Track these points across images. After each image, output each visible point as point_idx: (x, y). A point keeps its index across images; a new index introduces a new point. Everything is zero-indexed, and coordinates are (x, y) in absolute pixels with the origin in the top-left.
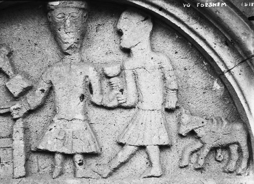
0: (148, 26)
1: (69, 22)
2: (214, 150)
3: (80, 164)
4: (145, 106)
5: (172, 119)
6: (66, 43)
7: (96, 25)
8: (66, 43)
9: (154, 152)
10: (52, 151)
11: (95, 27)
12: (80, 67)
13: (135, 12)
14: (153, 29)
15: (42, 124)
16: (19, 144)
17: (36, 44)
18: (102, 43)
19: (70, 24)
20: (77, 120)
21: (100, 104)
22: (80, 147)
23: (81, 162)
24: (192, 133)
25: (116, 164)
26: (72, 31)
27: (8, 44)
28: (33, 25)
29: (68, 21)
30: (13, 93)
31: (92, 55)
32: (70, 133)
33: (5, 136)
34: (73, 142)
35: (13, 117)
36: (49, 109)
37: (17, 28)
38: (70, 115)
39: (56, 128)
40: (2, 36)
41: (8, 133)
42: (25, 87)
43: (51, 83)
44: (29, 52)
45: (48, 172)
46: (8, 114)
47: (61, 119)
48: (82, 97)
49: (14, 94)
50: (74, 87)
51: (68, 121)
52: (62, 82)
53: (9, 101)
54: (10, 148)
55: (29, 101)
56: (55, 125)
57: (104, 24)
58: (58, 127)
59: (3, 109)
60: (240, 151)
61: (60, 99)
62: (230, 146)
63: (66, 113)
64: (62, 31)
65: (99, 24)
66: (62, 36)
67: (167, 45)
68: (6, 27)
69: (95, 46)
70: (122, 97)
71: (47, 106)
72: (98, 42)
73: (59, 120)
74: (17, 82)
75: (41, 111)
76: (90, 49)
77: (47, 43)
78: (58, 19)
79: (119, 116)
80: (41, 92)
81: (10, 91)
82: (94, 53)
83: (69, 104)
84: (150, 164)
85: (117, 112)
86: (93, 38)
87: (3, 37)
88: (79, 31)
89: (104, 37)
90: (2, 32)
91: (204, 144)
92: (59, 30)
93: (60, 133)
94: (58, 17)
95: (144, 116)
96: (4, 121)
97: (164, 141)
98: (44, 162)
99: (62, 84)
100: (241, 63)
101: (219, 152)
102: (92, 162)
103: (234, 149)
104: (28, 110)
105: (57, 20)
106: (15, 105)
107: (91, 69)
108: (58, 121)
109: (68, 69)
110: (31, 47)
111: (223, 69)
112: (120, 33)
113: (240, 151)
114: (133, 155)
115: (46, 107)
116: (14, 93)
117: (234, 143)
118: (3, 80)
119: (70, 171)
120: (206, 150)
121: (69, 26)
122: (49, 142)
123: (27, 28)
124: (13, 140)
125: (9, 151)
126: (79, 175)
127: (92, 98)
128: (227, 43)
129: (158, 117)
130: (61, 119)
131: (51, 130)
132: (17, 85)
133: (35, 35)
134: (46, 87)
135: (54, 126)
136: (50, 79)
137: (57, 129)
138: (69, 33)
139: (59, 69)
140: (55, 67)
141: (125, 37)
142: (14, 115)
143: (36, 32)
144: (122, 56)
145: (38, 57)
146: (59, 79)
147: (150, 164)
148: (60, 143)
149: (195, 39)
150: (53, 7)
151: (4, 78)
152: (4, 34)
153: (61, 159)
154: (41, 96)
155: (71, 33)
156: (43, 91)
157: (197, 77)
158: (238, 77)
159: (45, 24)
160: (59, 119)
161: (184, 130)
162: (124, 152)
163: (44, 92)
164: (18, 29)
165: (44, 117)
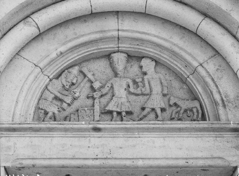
3: (124, 116)
4: (154, 92)
5: (166, 99)
11: (130, 66)
14: (156, 64)
43: (112, 84)
60: (198, 111)
95: (153, 97)
100: (212, 57)
113: (198, 111)
127: (130, 90)
129: (160, 97)
158: (225, 42)
161: (172, 103)
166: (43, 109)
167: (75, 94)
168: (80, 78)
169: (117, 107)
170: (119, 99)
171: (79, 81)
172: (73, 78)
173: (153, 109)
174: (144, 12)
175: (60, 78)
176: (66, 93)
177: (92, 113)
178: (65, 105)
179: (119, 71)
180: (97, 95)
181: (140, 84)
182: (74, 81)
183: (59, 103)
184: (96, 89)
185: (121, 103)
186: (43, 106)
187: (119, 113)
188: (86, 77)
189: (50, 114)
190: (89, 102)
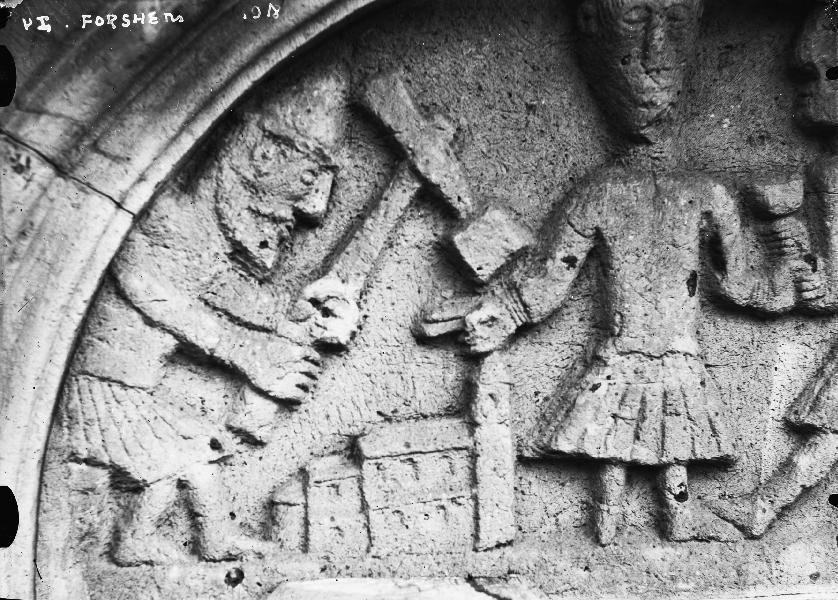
1: (662, 35)
6: (645, 105)
7: (719, 48)
8: (645, 105)
10: (601, 456)
12: (686, 184)
13: (279, 92)
15: (553, 368)
17: (530, 108)
18: (735, 108)
19: (662, 42)
20: (677, 355)
21: (744, 302)
23: (683, 488)
25: (791, 492)
26: (667, 66)
27: (445, 105)
28: (525, 42)
29: (659, 33)
30: (475, 269)
31: (703, 143)
32: (657, 398)
33: (435, 411)
34: (667, 425)
35: (472, 348)
36: (576, 319)
37: (474, 50)
38: (656, 340)
39: (611, 381)
40: (427, 78)
42: (515, 249)
44: (509, 132)
45: (570, 526)
47: (632, 352)
49: (478, 272)
50: (671, 247)
51: (651, 357)
52: (633, 232)
53: (449, 294)
54: (465, 451)
55: (527, 298)
56: (608, 371)
57: (743, 46)
58: (620, 380)
59: (436, 321)
61: (627, 286)
63: (643, 333)
64: (633, 65)
65: (730, 42)
66: (632, 80)
68: (440, 49)
69: (713, 116)
71: (571, 309)
72: (724, 102)
73: (623, 358)
74: (490, 234)
75: (553, 326)
76: (698, 126)
77: (565, 102)
78: (625, 25)
79: (791, 339)
80: (566, 265)
81: (460, 258)
82: (709, 139)
86: (708, 91)
87: (428, 82)
88: (683, 64)
89: (742, 88)
90: (427, 65)
92: (624, 63)
93: (627, 399)
94: (627, 17)
96: (432, 360)
98: (559, 493)
99: (633, 240)
104: (520, 323)
105: (624, 29)
106: (479, 307)
107: (719, 190)
108: (619, 358)
109: (651, 191)
110: (514, 116)
115: (569, 314)
116: (479, 269)
118: (430, 226)
119: (642, 520)
121: (659, 48)
122: (593, 429)
123: (504, 51)
124: (476, 424)
126: (681, 532)
130: (632, 352)
131: (595, 388)
132: (491, 241)
133: (528, 76)
135: (605, 377)
136: (598, 221)
137: (616, 386)
138: (658, 71)
139: (624, 189)
140: (609, 184)
142: (478, 341)
143: (533, 68)
145: (537, 147)
146: (623, 222)
148: (626, 432)
151: (435, 219)
152: (434, 72)
153: (622, 483)
154: (566, 278)
155: (662, 72)
156: (570, 261)
159: (561, 42)
160: (622, 354)
162: (817, 454)
163: (574, 267)
164: (478, 56)
165: (562, 348)
166: (102, 465)
167: (327, 313)
168: (357, 170)
169: (637, 437)
170: (648, 367)
171: (355, 193)
172: (308, 177)
174: (103, 147)
175: (206, 189)
176: (257, 303)
177: (462, 475)
178: (257, 414)
179: (649, 124)
180: (488, 320)
181: (793, 230)
182: (316, 204)
183: (213, 391)
184: (484, 274)
185: (660, 394)
186: (96, 439)
187: (646, 476)
188: (404, 166)
189: (160, 498)
190: (436, 374)
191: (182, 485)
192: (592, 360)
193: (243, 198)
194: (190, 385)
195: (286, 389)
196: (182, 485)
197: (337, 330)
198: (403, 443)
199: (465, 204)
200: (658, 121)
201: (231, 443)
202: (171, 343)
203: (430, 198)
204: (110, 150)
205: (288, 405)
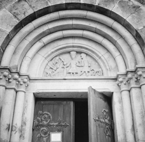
0: (86, 55)
2: (97, 72)
5: (89, 68)
9: (87, 72)
16: (65, 71)
22: (74, 72)
24: (93, 70)
41: (18, 93)
46: (64, 67)
48: (75, 65)
60: (101, 72)
62: (127, 141)
67: (89, 58)
70: (82, 65)
83: (73, 65)
84: (86, 74)
85: (81, 67)
91: (95, 71)
97: (88, 71)
101: (97, 72)
102: (77, 74)
103: (100, 72)
111: (97, 60)
112: (81, 56)
113: (101, 72)
114: (83, 73)
117: (100, 71)
120: (95, 72)
125: (63, 73)
128: (97, 56)
129: (88, 67)
134: (70, 63)
141: (82, 57)
144: (81, 60)
147: (86, 74)
149: (68, 2)
150: (49, 50)
157: (93, 62)
161: (92, 70)
173: (85, 72)
176: (54, 66)
178: (54, 71)
191: (50, 74)
192: (70, 68)
193: (54, 61)
194: (51, 70)
195: (55, 69)
196: (50, 74)
197: (58, 67)
198: (78, 73)
199: (64, 62)
200: (74, 58)
201: (52, 72)
202: (50, 67)
203: (63, 62)
204: (54, 107)
205: (55, 70)
